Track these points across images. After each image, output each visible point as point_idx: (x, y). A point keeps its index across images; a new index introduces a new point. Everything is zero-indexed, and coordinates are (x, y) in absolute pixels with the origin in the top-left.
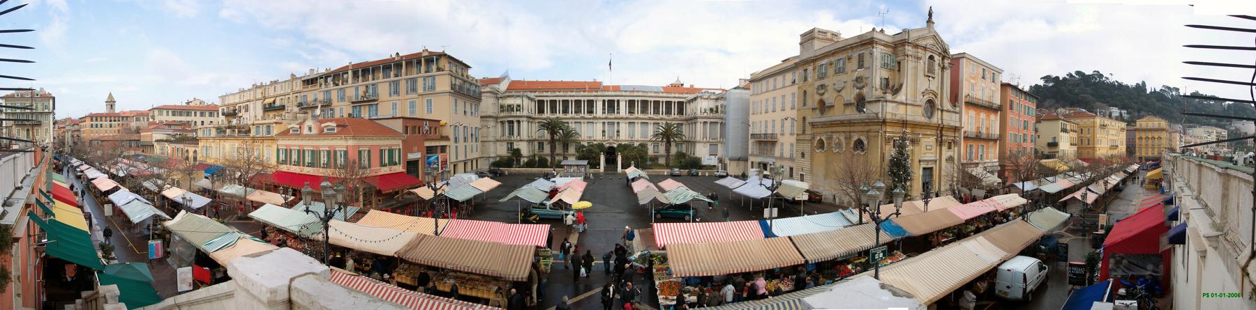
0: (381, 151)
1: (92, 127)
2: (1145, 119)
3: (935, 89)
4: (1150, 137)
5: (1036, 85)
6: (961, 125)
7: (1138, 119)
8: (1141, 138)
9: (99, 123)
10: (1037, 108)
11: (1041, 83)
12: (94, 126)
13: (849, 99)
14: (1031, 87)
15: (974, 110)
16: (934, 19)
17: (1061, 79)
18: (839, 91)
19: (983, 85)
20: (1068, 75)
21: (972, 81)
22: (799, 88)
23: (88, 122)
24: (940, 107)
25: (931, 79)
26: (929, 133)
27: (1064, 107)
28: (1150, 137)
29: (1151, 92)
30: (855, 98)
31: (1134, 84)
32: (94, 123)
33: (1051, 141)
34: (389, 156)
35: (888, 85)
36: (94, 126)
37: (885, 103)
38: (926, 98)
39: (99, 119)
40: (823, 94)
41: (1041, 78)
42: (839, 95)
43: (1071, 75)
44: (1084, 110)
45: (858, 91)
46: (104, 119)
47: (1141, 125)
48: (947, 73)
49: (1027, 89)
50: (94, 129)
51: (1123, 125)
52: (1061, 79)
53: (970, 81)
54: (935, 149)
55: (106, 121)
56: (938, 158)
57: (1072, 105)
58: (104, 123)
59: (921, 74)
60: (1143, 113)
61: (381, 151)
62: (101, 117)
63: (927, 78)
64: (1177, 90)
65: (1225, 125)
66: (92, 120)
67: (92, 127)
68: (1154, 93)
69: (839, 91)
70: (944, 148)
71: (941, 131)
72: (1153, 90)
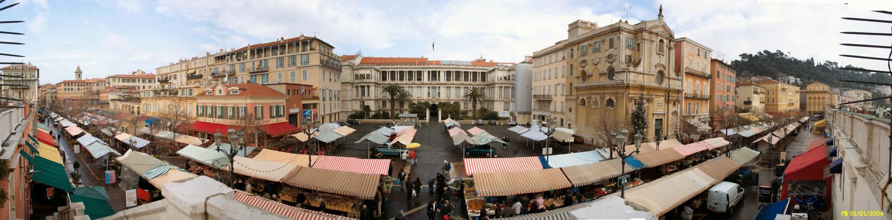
0: (271, 107)
1: (65, 90)
2: (813, 85)
3: (664, 63)
4: (817, 97)
5: (736, 60)
6: (683, 88)
7: (808, 84)
8: (810, 98)
9: (70, 87)
10: (737, 76)
11: (740, 59)
12: (67, 89)
13: (603, 70)
14: (732, 61)
15: (693, 79)
16: (663, 13)
17: (753, 56)
18: (596, 65)
19: (698, 60)
20: (758, 53)
21: (690, 57)
22: (567, 62)
23: (63, 87)
24: (667, 76)
25: (661, 56)
26: (659, 94)
27: (755, 76)
28: (817, 97)
29: (817, 66)
30: (607, 70)
31: (805, 60)
32: (67, 87)
33: (746, 100)
34: (276, 110)
35: (631, 60)
36: (67, 89)
37: (628, 73)
38: (658, 69)
39: (70, 84)
40: (585, 66)
41: (740, 56)
42: (596, 68)
43: (760, 53)
44: (770, 78)
45: (609, 64)
46: (74, 84)
47: (810, 89)
48: (673, 52)
49: (729, 63)
50: (67, 91)
51: (798, 89)
52: (753, 56)
53: (689, 58)
54: (664, 105)
55: (75, 86)
56: (666, 112)
57: (761, 74)
58: (74, 87)
59: (654, 52)
60: (811, 80)
61: (271, 107)
62: (72, 83)
63: (658, 55)
64: (836, 64)
65: (870, 89)
66: (65, 85)
67: (65, 90)
68: (820, 66)
69: (596, 65)
70: (671, 105)
71: (669, 93)
72: (819, 64)
